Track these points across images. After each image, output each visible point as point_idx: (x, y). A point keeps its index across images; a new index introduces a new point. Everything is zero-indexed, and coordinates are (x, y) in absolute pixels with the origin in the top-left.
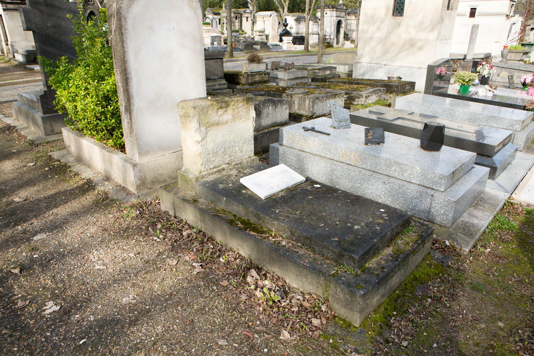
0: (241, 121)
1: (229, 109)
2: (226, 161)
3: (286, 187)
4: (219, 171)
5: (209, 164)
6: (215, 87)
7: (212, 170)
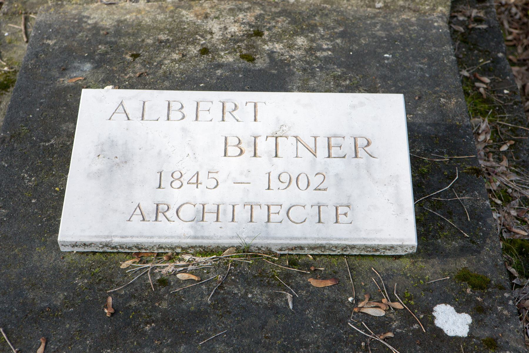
3: (236, 242)
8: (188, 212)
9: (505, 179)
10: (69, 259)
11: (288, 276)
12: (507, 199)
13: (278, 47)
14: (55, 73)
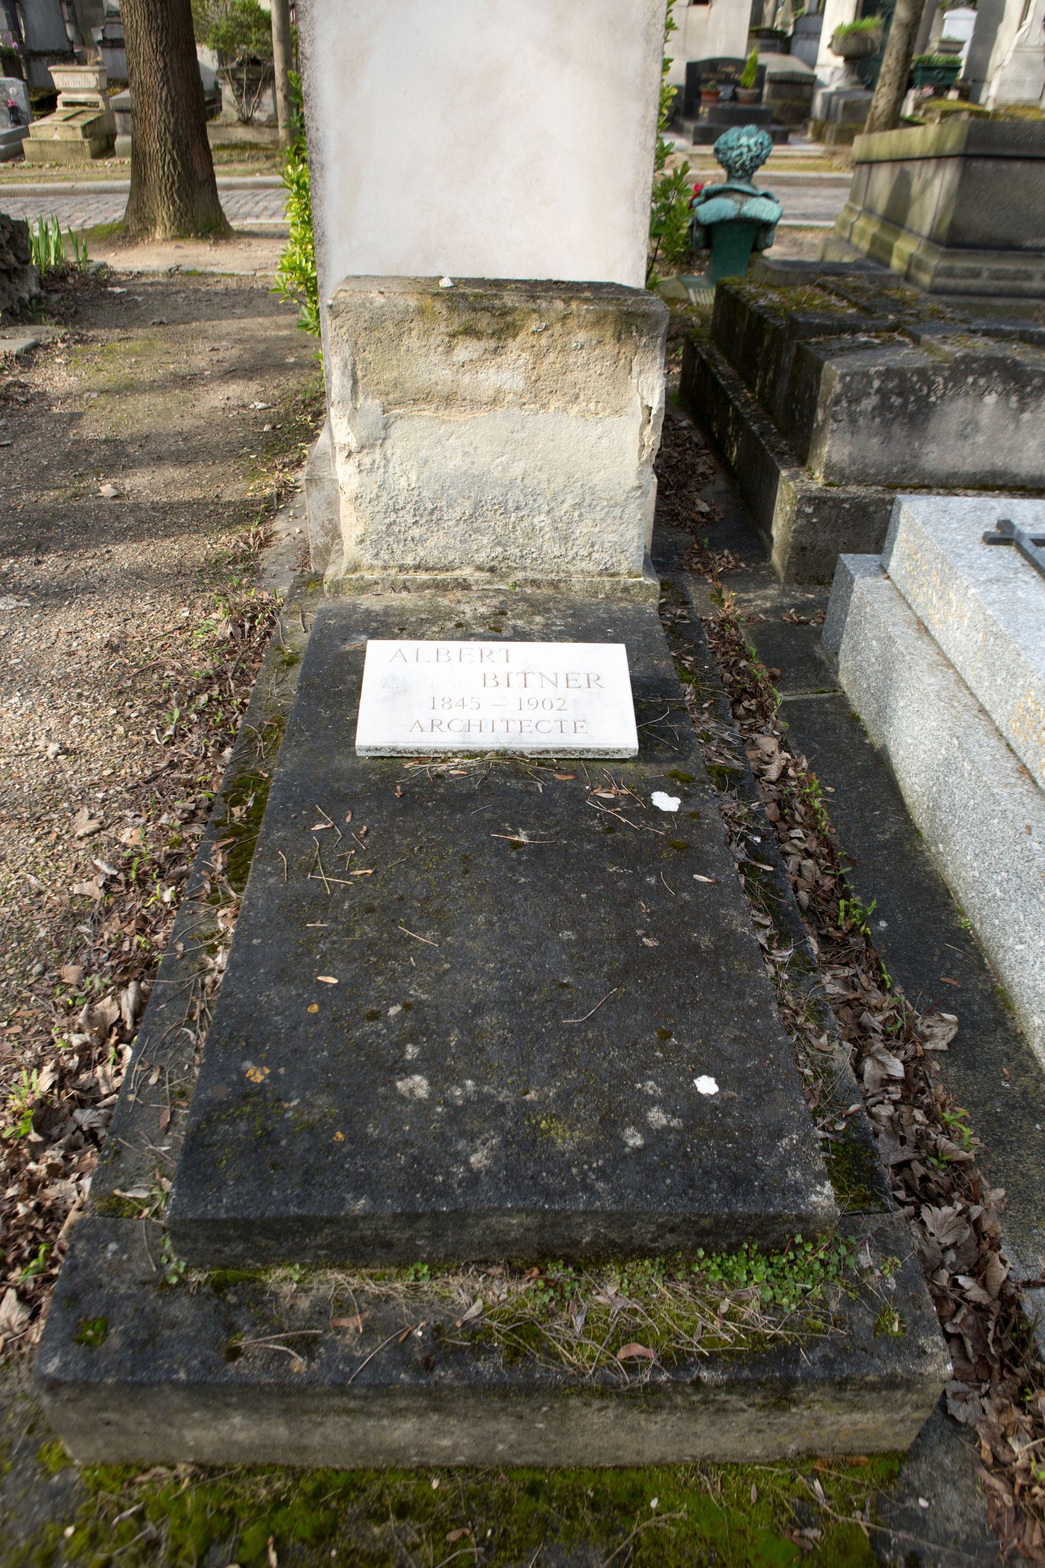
0: (574, 410)
1: (513, 345)
2: (481, 558)
3: (497, 746)
4: (441, 587)
5: (398, 549)
6: (1026, 285)
7: (411, 575)
8: (456, 726)
9: (706, 726)
10: (363, 762)
11: (537, 773)
12: (709, 739)
13: (520, 623)
14: (337, 642)
